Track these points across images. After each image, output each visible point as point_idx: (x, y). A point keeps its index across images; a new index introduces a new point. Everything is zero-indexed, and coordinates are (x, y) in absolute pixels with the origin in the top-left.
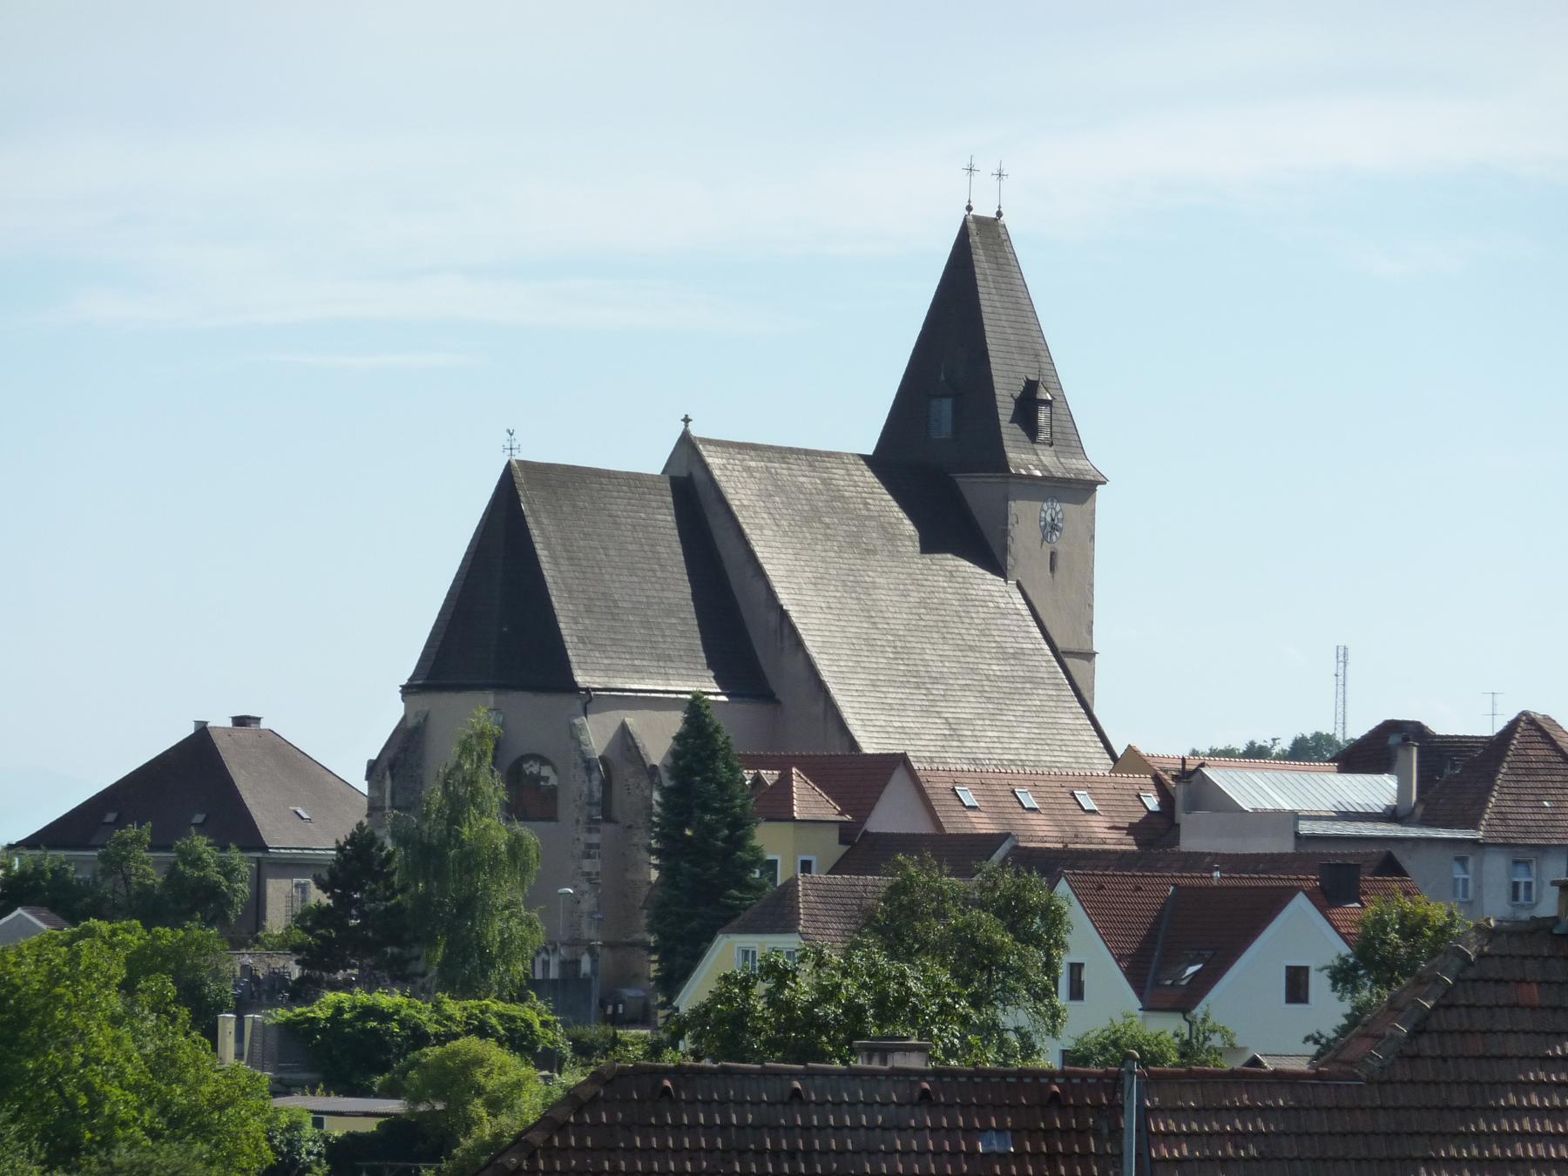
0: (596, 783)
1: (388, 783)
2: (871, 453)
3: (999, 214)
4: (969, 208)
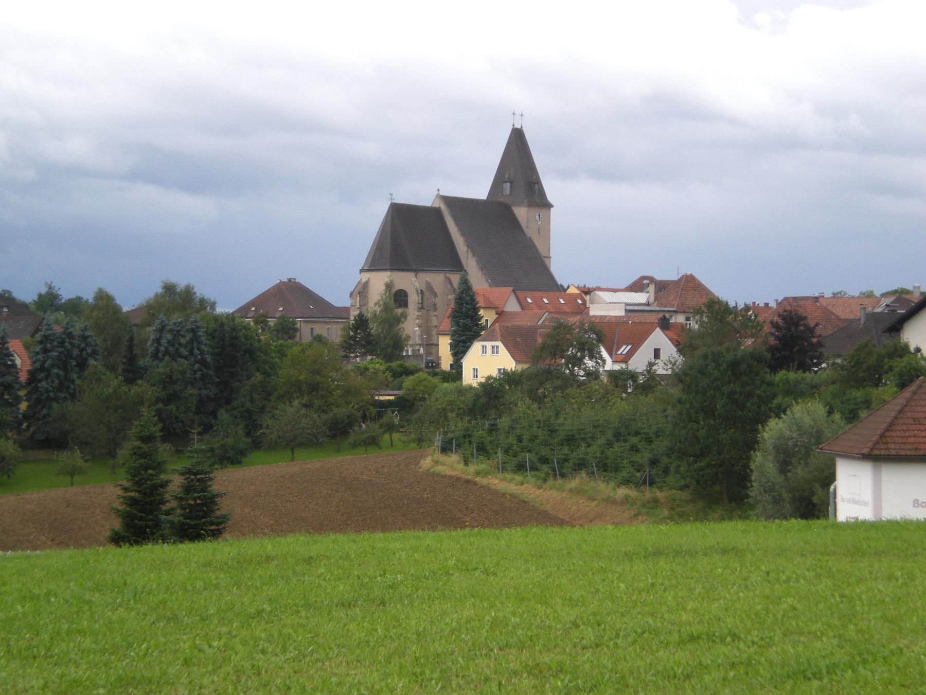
0: (420, 298)
1: (358, 298)
2: (125, 309)
3: (522, 127)
4: (513, 126)
